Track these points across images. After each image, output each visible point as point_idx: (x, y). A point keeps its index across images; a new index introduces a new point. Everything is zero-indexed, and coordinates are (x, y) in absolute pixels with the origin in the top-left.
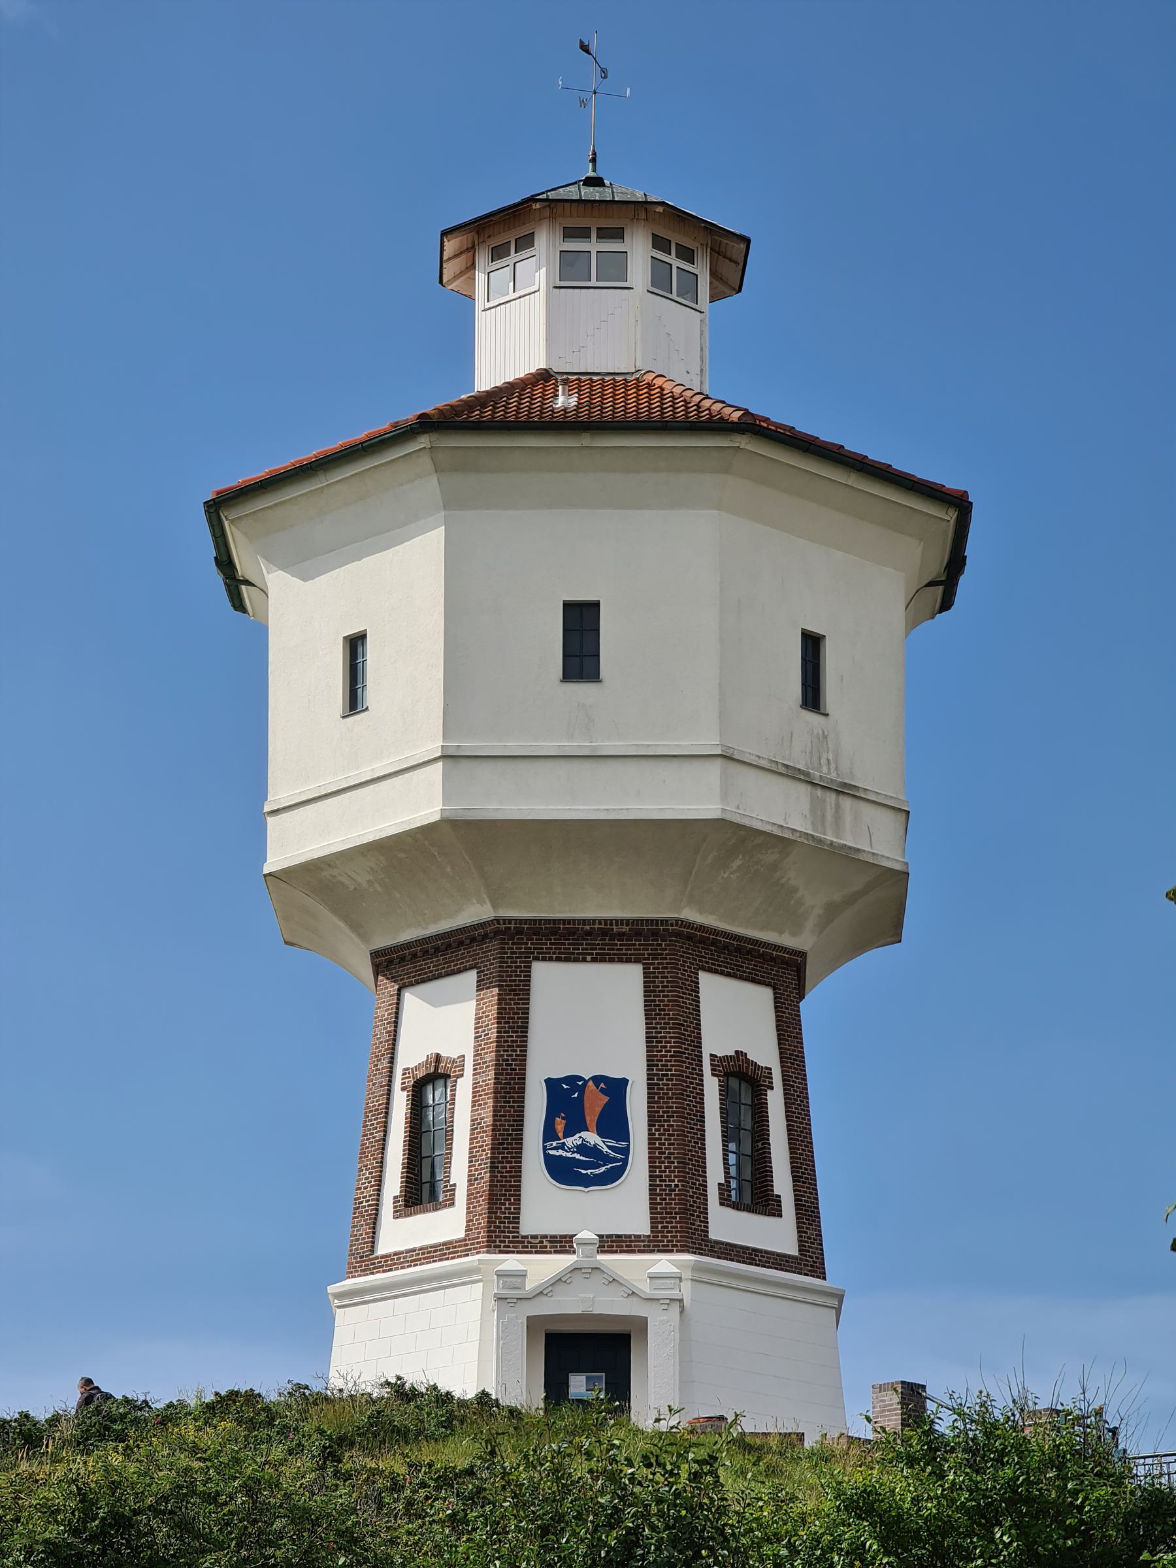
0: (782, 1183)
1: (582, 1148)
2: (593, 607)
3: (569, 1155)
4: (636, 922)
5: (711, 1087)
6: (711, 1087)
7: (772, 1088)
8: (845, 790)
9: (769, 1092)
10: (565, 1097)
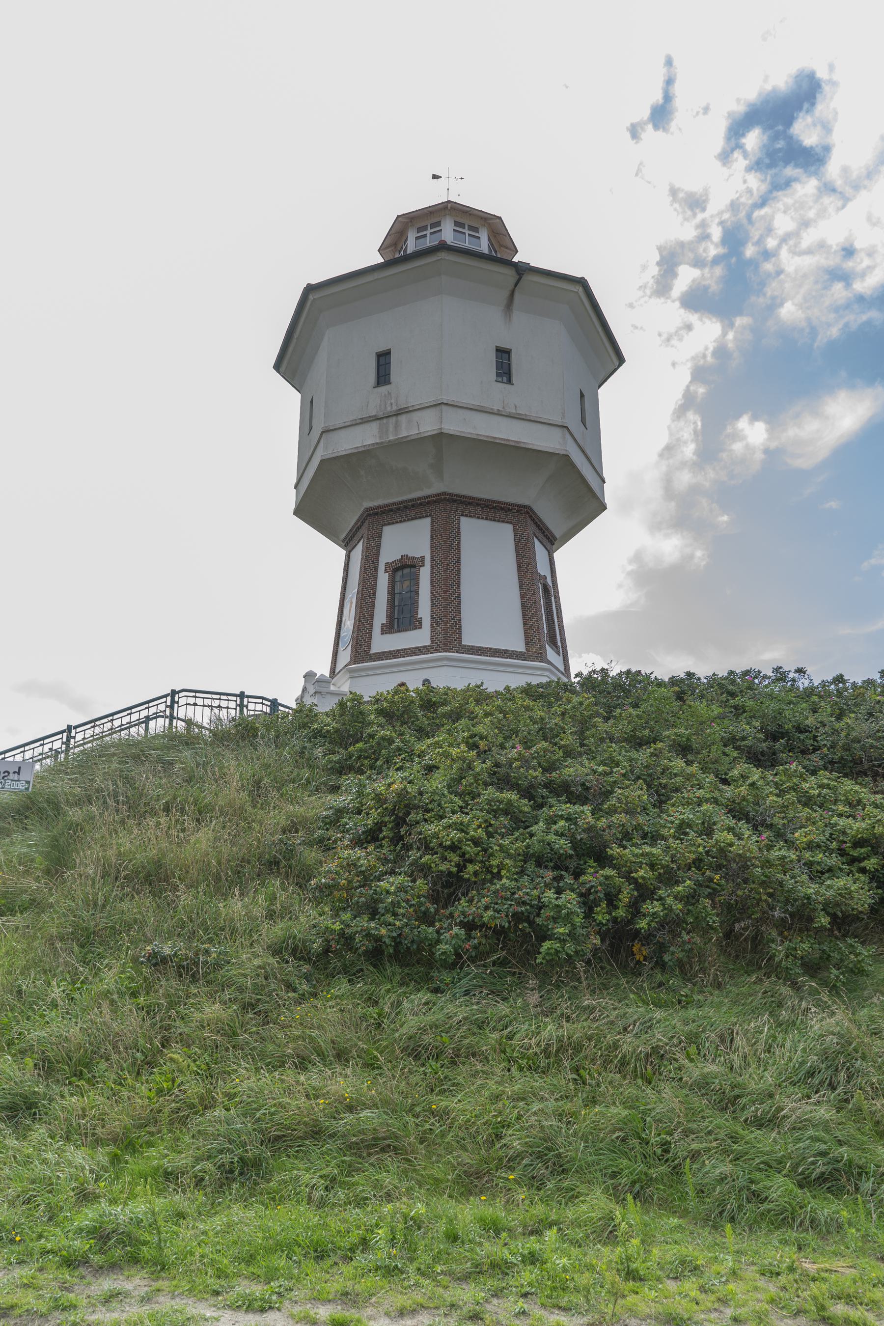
5: (383, 579)
6: (383, 579)
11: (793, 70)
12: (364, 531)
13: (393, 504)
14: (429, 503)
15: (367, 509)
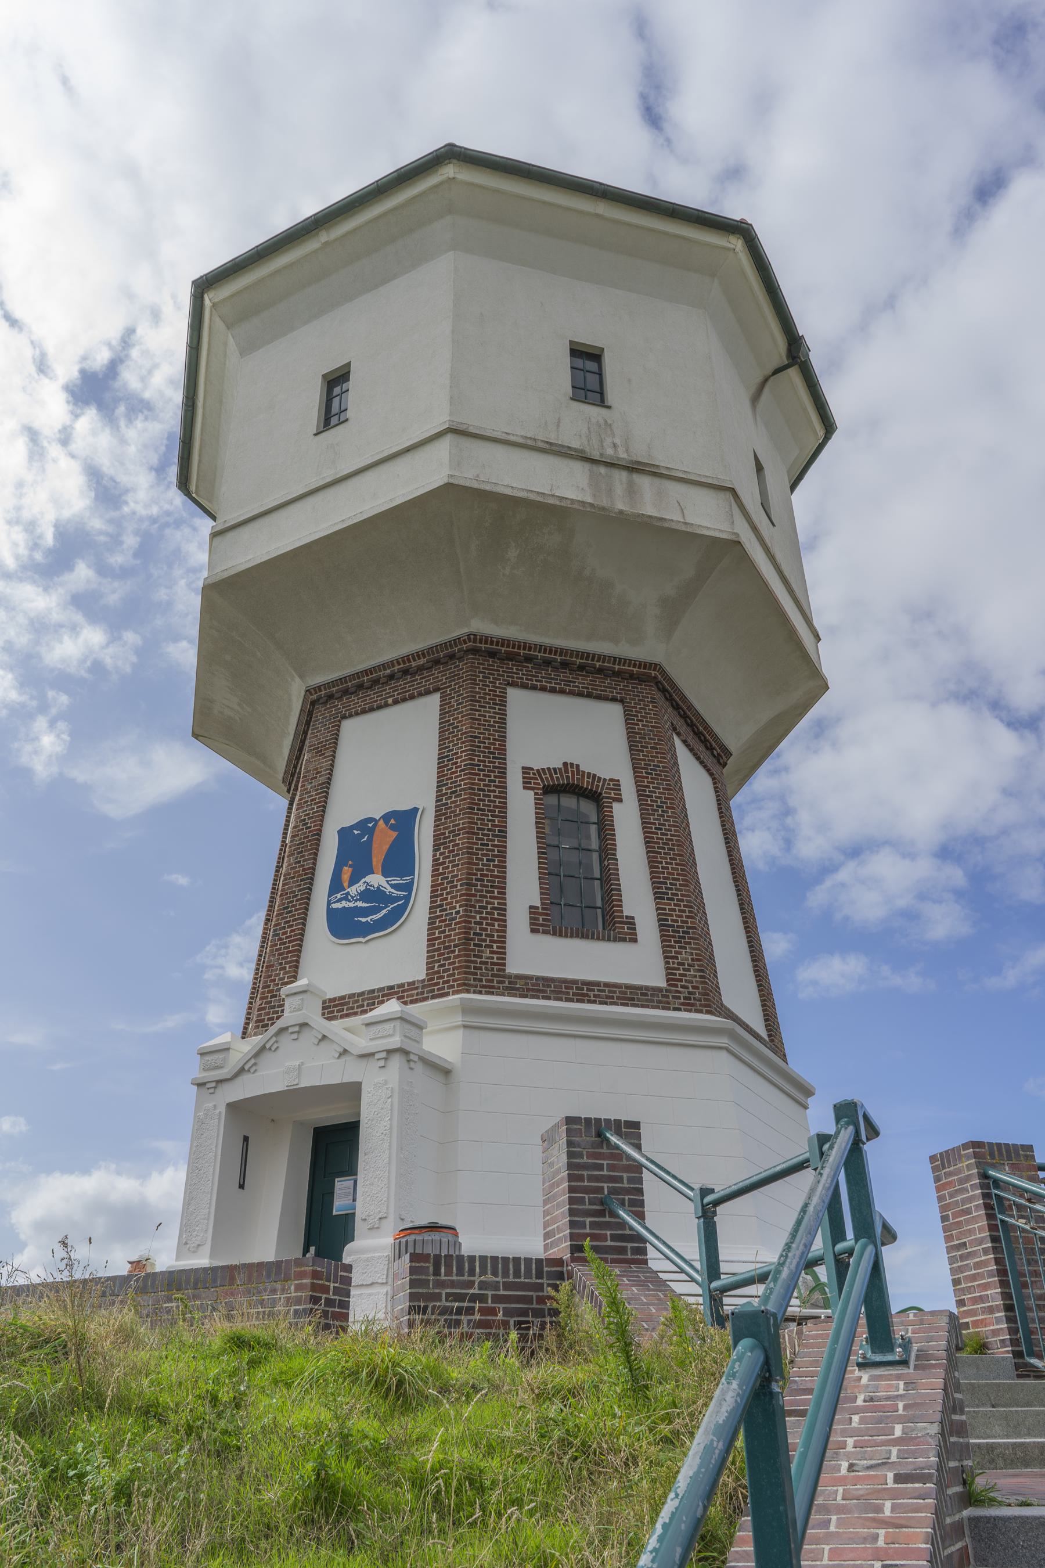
0: (637, 898)
1: (366, 895)
2: (567, 1118)
3: (351, 905)
4: (431, 650)
5: (522, 807)
6: (522, 807)
7: (621, 800)
8: (634, 468)
9: (615, 805)
10: (355, 845)
13: (540, 648)
15: (473, 637)
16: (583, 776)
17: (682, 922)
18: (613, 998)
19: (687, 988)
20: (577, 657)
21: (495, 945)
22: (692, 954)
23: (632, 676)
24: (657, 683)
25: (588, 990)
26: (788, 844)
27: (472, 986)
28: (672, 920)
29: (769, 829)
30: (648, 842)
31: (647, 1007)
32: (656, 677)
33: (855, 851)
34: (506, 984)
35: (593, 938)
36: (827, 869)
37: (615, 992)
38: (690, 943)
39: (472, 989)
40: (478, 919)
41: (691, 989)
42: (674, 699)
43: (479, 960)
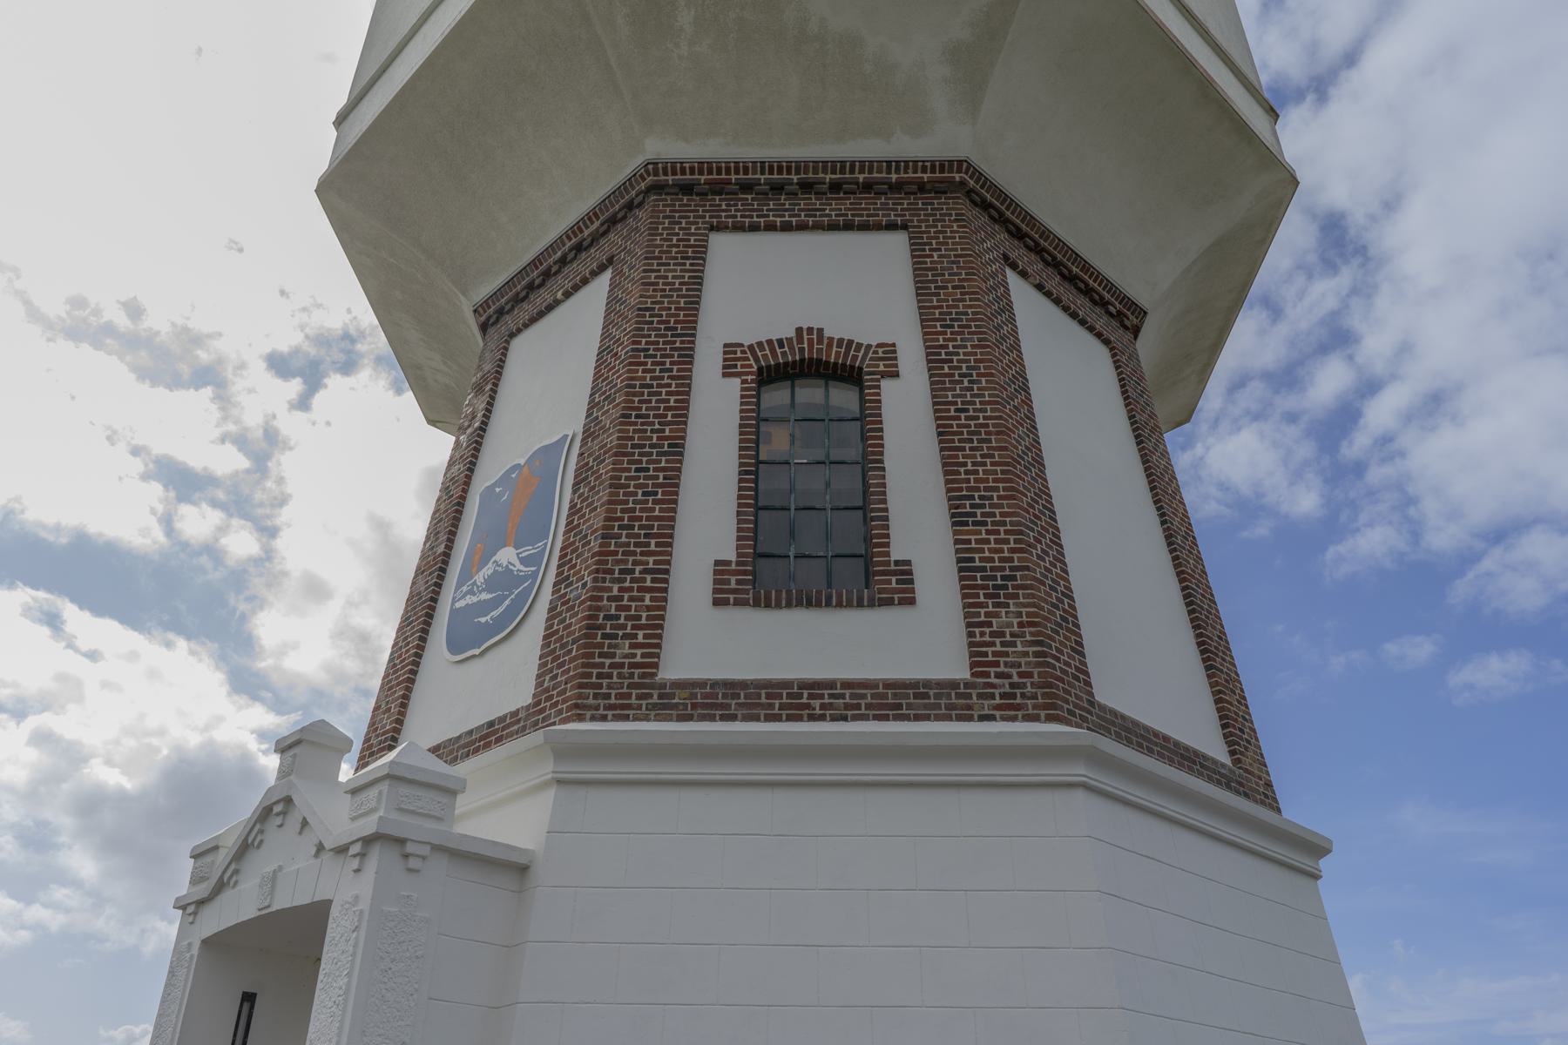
0: (919, 526)
3: (475, 599)
5: (716, 407)
6: (716, 407)
9: (886, 384)
11: (144, 484)
12: (629, 241)
14: (897, 187)
15: (652, 167)
16: (830, 345)
17: (1002, 560)
18: (858, 707)
19: (1009, 676)
20: (825, 171)
21: (641, 634)
22: (1019, 614)
23: (922, 187)
24: (970, 193)
25: (811, 696)
26: (1415, 531)
27: (589, 707)
28: (981, 560)
29: (1390, 523)
30: (943, 433)
31: (927, 718)
32: (963, 183)
33: (1501, 534)
34: (655, 699)
35: (828, 604)
36: (1467, 559)
37: (863, 696)
38: (1016, 596)
39: (589, 714)
40: (615, 592)
41: (1016, 679)
42: (1008, 221)
43: (608, 662)
